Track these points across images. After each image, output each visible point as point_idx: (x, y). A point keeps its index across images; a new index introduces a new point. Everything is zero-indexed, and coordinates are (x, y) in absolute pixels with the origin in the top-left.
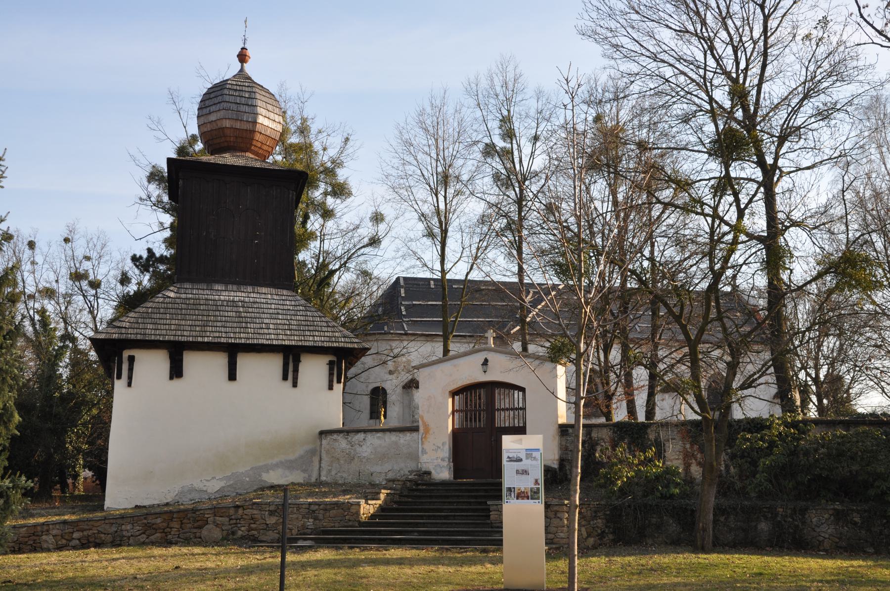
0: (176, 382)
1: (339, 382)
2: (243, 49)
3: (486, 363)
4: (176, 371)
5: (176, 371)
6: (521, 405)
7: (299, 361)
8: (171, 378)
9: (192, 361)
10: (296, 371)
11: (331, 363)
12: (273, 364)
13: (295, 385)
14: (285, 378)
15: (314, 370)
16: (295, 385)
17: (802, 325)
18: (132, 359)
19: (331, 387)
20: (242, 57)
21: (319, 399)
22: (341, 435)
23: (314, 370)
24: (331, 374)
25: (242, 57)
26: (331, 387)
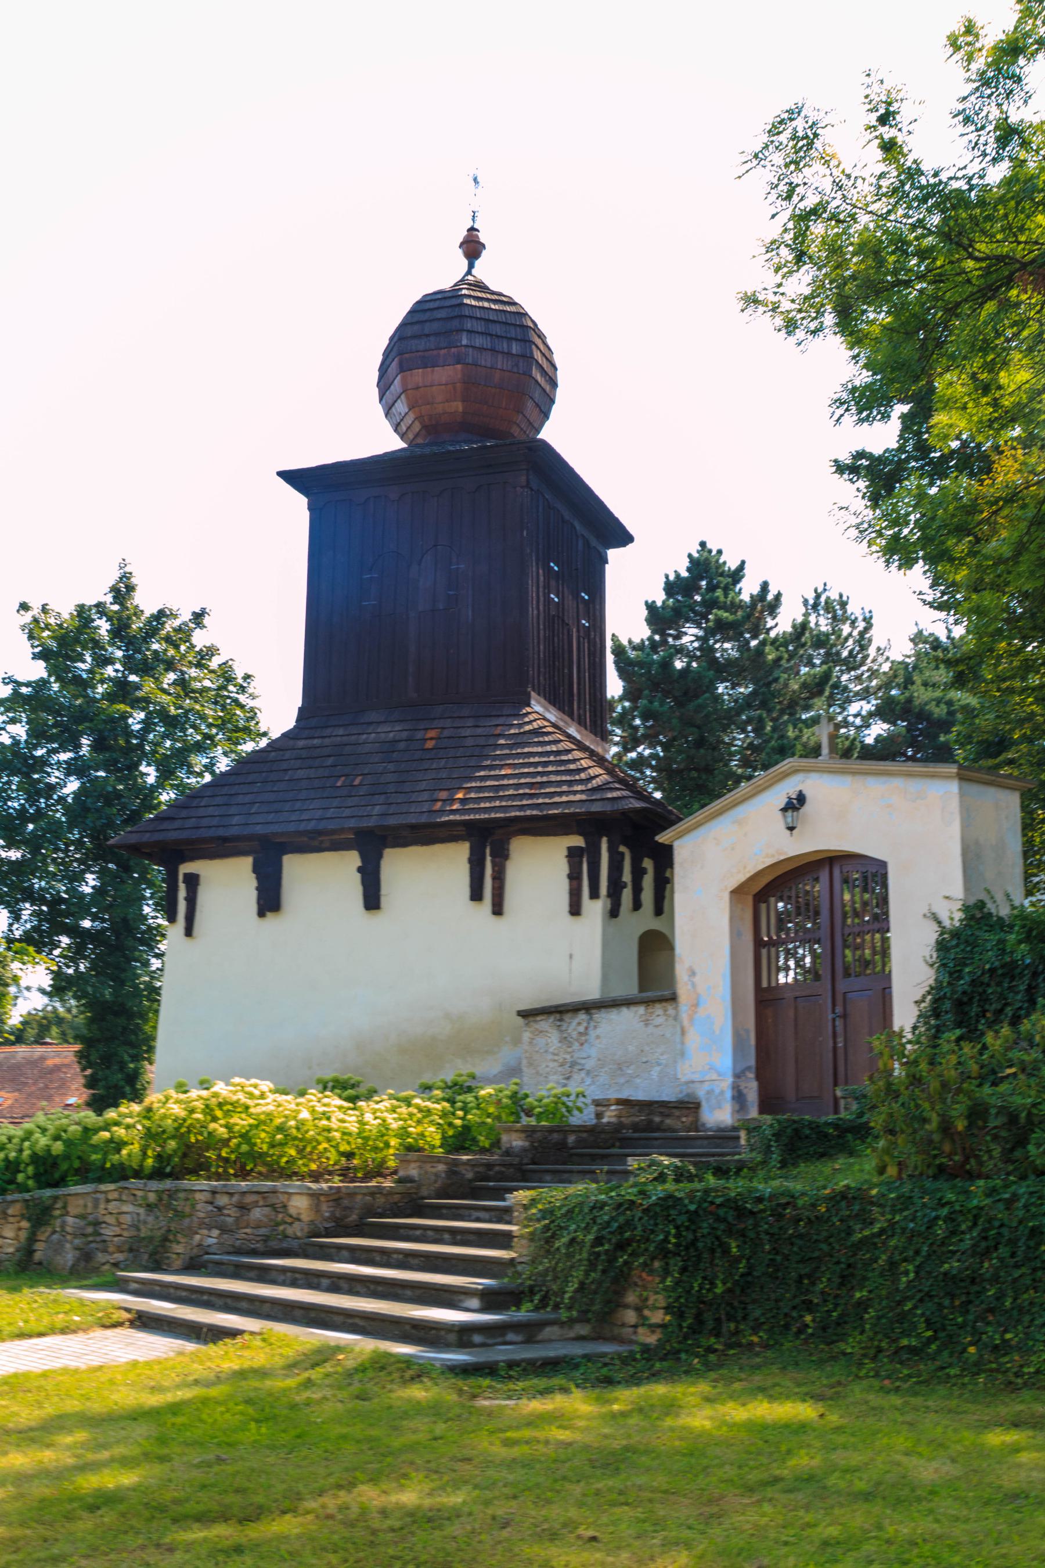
0: (272, 920)
1: (594, 895)
2: (472, 229)
3: (796, 804)
4: (269, 901)
5: (269, 901)
6: (764, 952)
7: (506, 857)
8: (261, 914)
9: (299, 871)
10: (499, 878)
11: (573, 854)
12: (453, 862)
13: (498, 910)
14: (476, 895)
15: (539, 869)
16: (498, 910)
17: (248, 1532)
18: (192, 881)
19: (575, 910)
20: (472, 247)
21: (546, 930)
22: (552, 1019)
23: (539, 869)
24: (574, 877)
25: (472, 247)
26: (575, 910)
